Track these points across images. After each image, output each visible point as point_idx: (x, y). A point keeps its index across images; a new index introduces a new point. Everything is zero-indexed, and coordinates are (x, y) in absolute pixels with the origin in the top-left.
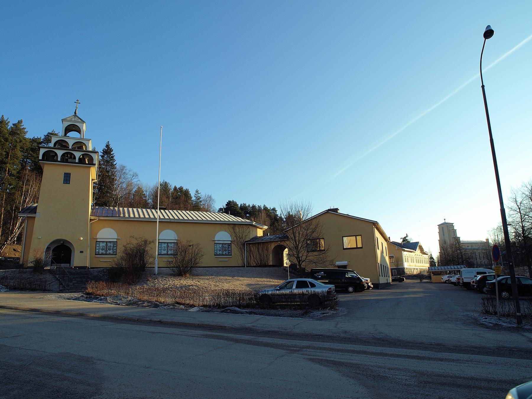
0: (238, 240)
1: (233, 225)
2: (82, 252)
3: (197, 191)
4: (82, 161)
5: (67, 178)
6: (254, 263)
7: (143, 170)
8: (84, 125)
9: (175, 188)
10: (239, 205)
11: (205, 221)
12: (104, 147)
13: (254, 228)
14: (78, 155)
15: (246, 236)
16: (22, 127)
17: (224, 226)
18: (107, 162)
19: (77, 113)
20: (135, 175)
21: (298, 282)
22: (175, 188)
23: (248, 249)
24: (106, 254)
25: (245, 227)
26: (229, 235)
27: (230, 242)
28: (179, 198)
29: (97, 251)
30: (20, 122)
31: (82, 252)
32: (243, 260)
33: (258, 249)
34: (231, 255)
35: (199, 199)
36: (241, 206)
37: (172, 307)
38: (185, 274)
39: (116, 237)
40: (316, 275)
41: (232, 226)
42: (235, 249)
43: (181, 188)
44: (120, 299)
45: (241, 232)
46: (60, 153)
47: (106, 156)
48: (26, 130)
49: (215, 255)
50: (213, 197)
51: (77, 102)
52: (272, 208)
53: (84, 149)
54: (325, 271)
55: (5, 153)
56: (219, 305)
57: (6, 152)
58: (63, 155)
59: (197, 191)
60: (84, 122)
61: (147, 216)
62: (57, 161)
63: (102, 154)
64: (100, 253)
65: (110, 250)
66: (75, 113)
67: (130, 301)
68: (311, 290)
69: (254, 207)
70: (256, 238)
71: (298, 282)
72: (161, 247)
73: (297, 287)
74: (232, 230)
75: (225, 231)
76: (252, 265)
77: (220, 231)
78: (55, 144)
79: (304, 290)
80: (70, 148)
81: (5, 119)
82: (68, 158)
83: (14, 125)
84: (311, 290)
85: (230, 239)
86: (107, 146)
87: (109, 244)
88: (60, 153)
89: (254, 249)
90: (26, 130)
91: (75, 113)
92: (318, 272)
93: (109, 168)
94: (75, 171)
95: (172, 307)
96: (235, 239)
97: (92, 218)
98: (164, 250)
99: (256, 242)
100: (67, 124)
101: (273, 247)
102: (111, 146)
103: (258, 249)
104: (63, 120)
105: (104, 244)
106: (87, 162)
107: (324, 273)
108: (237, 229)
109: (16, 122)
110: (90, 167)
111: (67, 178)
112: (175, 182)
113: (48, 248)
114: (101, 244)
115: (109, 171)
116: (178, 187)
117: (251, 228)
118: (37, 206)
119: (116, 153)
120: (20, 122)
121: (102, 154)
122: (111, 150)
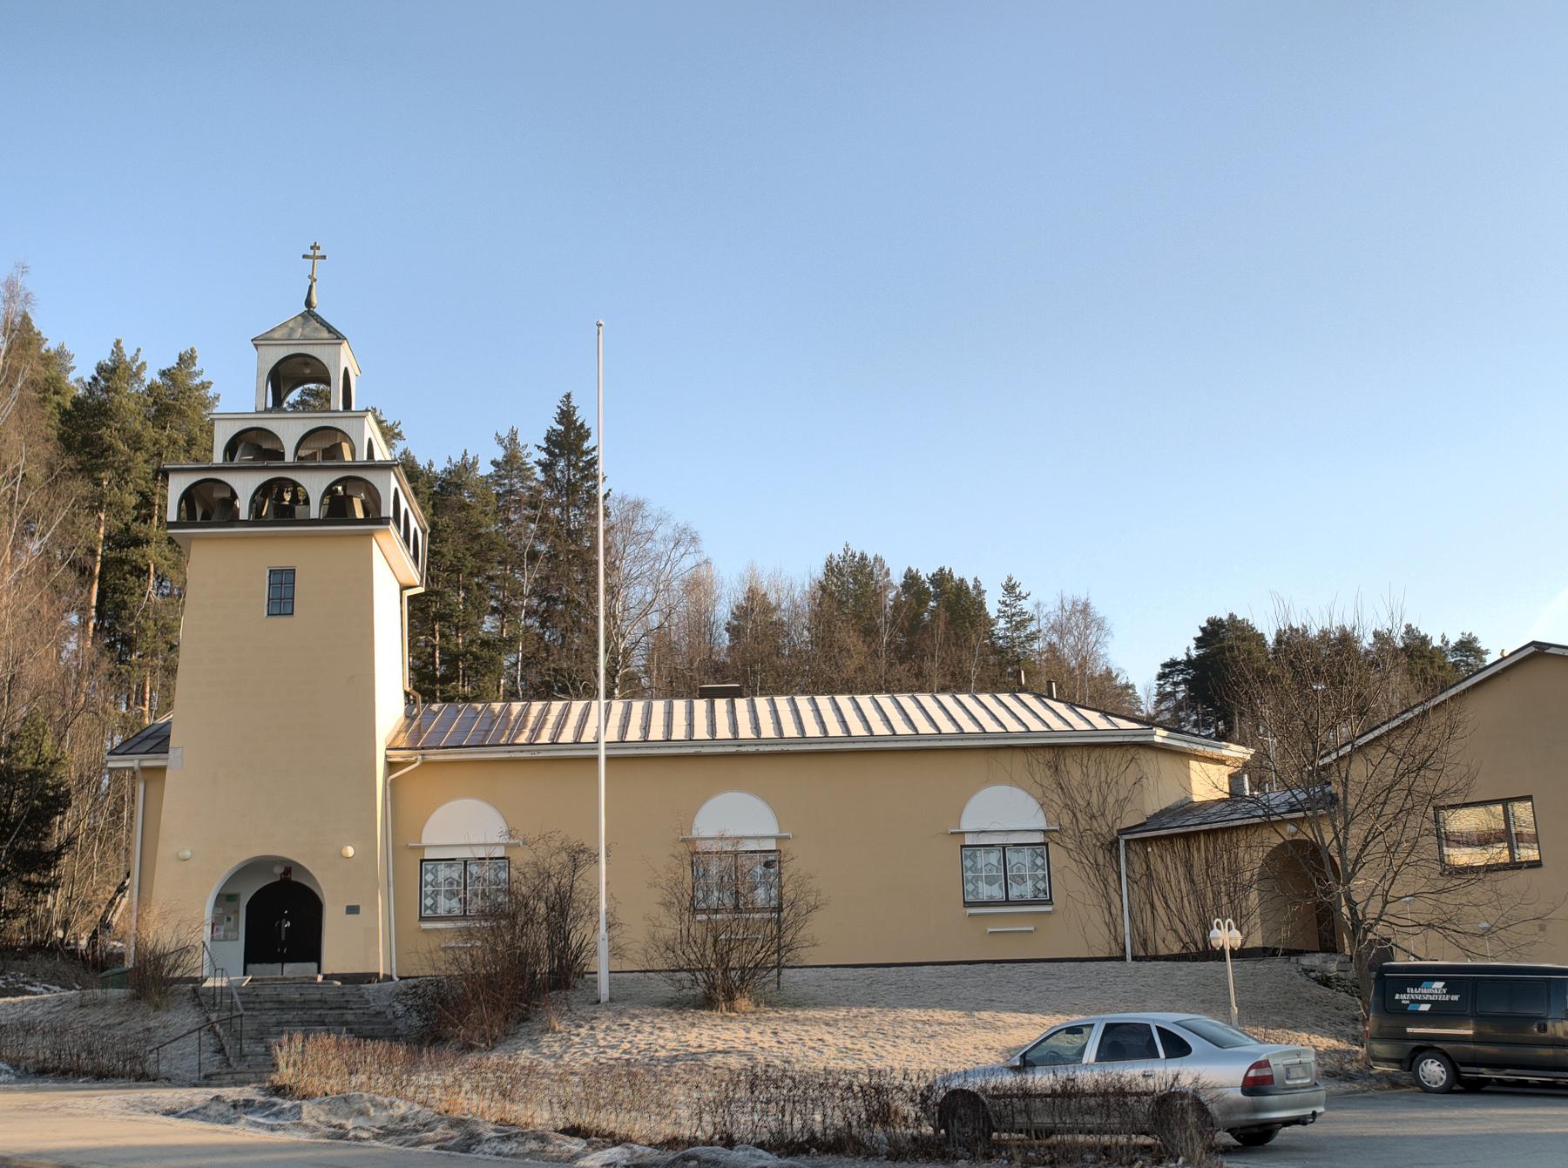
0: (1083, 824)
1: (1053, 752)
2: (353, 910)
3: (1010, 588)
4: (337, 508)
5: (282, 592)
6: (1171, 937)
7: (730, 506)
8: (345, 347)
9: (912, 580)
10: (1270, 639)
11: (994, 735)
12: (549, 421)
13: (1166, 763)
14: (315, 485)
15: (1121, 803)
16: (197, 381)
17: (1004, 757)
18: (572, 489)
19: (315, 300)
20: (686, 538)
21: (1110, 1028)
22: (912, 580)
23: (1139, 867)
24: (1007, 902)
25: (1113, 757)
26: (1031, 805)
27: (1039, 838)
28: (926, 631)
29: (429, 902)
30: (186, 360)
31: (353, 910)
32: (1113, 924)
33: (1189, 866)
34: (1050, 902)
35: (1021, 625)
36: (1279, 641)
37: (534, 1145)
38: (730, 998)
39: (775, 831)
40: (1404, 998)
41: (1049, 755)
42: (1072, 878)
43: (941, 578)
44: (362, 1113)
45: (1093, 783)
46: (245, 486)
47: (562, 464)
48: (211, 393)
49: (967, 904)
50: (1099, 608)
51: (314, 254)
52: (1454, 639)
53: (348, 457)
54: (1454, 977)
55: (133, 500)
56: (730, 1137)
57: (142, 494)
58: (264, 490)
59: (1010, 588)
60: (338, 337)
61: (857, 729)
62: (232, 519)
63: (544, 456)
64: (441, 911)
65: (1021, 879)
66: (308, 303)
67: (403, 1119)
68: (1159, 1073)
69: (1345, 641)
70: (1187, 808)
71: (1110, 1028)
72: (974, 868)
73: (1100, 1057)
74: (1043, 775)
75: (1013, 781)
76: (1163, 951)
77: (988, 782)
78: (231, 448)
79: (1131, 1072)
80: (289, 457)
81: (128, 353)
82: (279, 506)
83: (163, 374)
84: (1159, 1073)
85: (1043, 825)
86: (566, 416)
87: (474, 869)
88: (245, 486)
89: (1167, 866)
90: (211, 393)
91: (308, 303)
92: (1417, 983)
93: (576, 518)
94: (311, 556)
95: (534, 1145)
96: (1066, 820)
97: (397, 756)
98: (990, 881)
99: (1184, 830)
100: (277, 354)
101: (1259, 855)
102: (581, 416)
103: (1189, 866)
104: (258, 342)
105: (455, 873)
106: (360, 514)
107: (1451, 987)
108: (1074, 770)
109: (171, 362)
110: (370, 534)
111: (282, 592)
112: (906, 552)
113: (225, 899)
114: (444, 872)
115: (579, 532)
116: (926, 571)
117: (1148, 761)
118: (169, 723)
119: (604, 444)
120: (186, 360)
121: (544, 456)
122: (582, 434)
